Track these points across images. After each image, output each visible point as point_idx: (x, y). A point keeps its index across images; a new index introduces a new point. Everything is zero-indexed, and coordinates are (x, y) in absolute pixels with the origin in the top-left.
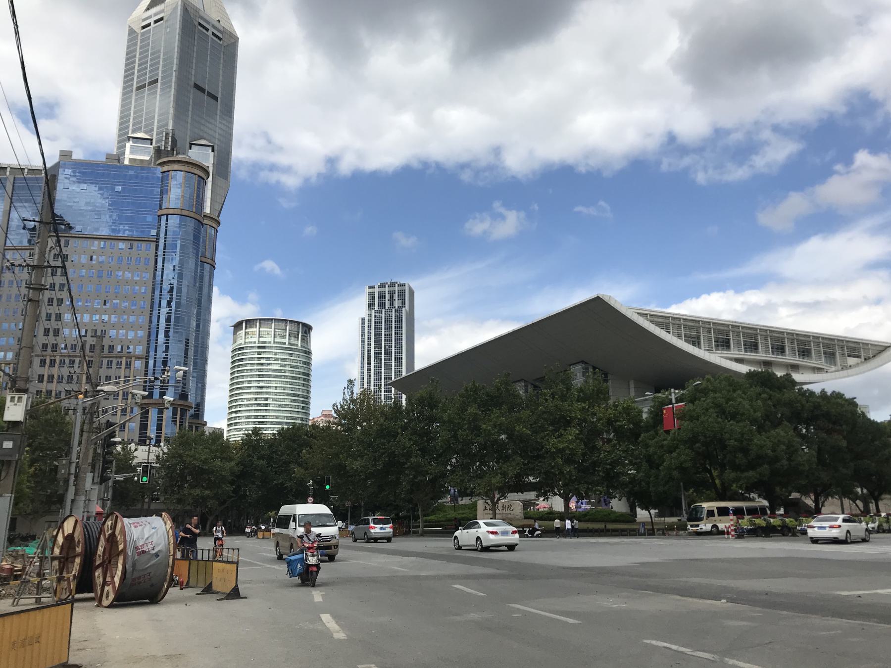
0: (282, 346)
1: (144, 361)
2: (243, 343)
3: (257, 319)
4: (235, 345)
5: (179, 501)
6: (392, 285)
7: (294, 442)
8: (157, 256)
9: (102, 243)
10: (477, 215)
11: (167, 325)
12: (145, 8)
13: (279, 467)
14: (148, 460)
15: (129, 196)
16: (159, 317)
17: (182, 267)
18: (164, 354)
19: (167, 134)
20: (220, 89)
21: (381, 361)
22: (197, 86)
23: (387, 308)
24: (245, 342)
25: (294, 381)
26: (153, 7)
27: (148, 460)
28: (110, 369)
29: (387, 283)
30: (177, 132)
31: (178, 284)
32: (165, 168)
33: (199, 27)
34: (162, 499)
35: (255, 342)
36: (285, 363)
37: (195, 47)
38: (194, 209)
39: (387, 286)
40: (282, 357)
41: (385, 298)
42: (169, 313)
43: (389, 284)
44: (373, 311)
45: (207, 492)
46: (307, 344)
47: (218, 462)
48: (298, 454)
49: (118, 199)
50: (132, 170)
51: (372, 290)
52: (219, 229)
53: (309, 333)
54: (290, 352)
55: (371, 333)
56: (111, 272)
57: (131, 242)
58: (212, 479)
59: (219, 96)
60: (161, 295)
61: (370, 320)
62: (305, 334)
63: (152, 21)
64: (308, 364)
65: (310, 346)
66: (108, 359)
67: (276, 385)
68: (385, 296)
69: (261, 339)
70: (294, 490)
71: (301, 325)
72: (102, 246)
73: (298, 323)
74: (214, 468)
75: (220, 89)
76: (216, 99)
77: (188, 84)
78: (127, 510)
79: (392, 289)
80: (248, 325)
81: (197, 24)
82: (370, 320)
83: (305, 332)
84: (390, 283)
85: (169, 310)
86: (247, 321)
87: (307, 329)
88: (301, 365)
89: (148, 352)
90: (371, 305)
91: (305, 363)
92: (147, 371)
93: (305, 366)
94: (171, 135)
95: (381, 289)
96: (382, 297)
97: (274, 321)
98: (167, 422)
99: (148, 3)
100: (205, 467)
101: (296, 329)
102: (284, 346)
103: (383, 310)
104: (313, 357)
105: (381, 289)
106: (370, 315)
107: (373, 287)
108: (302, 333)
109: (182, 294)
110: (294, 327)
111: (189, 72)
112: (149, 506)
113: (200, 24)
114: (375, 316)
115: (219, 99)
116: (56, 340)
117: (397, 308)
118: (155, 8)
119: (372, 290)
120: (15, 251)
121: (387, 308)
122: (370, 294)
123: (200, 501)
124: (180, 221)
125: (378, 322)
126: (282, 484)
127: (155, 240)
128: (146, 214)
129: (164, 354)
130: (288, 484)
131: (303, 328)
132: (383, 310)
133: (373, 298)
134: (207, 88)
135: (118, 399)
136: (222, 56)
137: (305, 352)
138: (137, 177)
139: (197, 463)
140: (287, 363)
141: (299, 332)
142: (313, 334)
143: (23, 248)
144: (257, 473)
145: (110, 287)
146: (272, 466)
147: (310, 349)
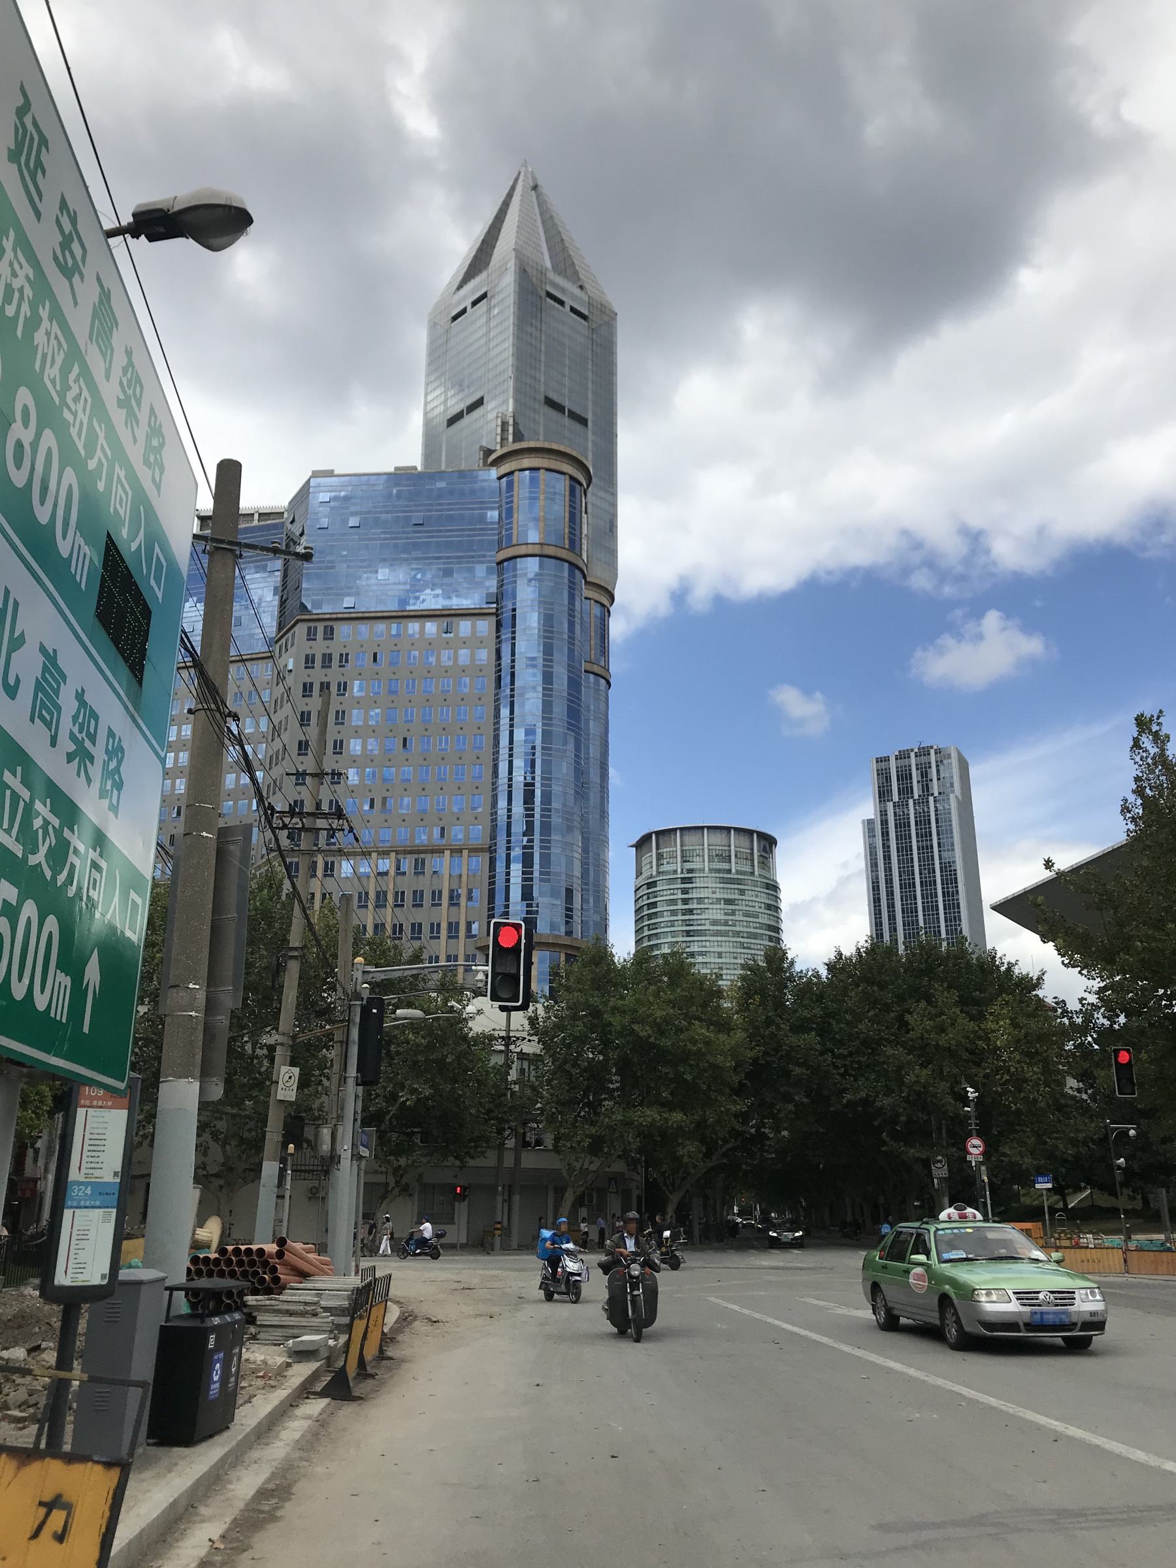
0: (725, 876)
1: (487, 855)
2: (654, 873)
3: (675, 830)
4: (640, 878)
5: (596, 1147)
6: (924, 752)
7: (882, 986)
8: (500, 670)
9: (394, 626)
10: (280, 1428)
11: (526, 809)
12: (456, 286)
13: (851, 1054)
14: (508, 1030)
15: (440, 531)
16: (507, 888)
17: (552, 632)
18: (525, 839)
19: (504, 425)
20: (590, 406)
21: (915, 899)
22: (550, 403)
23: (916, 797)
24: (659, 873)
25: (753, 941)
26: (469, 280)
27: (508, 1030)
28: (421, 877)
29: (912, 750)
30: (521, 421)
31: (543, 725)
32: (505, 468)
33: (548, 300)
34: (549, 1140)
35: (675, 872)
36: (733, 907)
37: (543, 345)
38: (567, 542)
39: (912, 755)
40: (726, 896)
41: (911, 779)
42: (528, 847)
43: (916, 750)
44: (890, 805)
45: (677, 1117)
46: (769, 872)
47: (701, 1031)
48: (900, 1019)
49: (419, 538)
50: (441, 479)
51: (883, 765)
52: (611, 609)
53: (771, 852)
54: (740, 887)
55: (889, 847)
56: (414, 681)
57: (449, 619)
58: (688, 1077)
59: (590, 417)
60: (509, 842)
61: (884, 823)
62: (763, 854)
63: (468, 303)
64: (774, 908)
65: (774, 874)
66: (416, 856)
67: (720, 950)
68: (911, 774)
69: (688, 866)
70: (903, 1119)
71: (755, 836)
72: (394, 632)
73: (750, 833)
74: (690, 1046)
75: (590, 406)
76: (583, 421)
77: (535, 399)
78: (461, 1168)
79: (923, 759)
80: (661, 841)
81: (543, 294)
82: (884, 823)
83: (765, 850)
84: (919, 749)
85: (529, 841)
86: (658, 833)
87: (768, 842)
88: (762, 910)
89: (493, 837)
90: (883, 794)
91: (769, 907)
92: (494, 876)
93: (769, 912)
94: (511, 422)
95: (901, 762)
96: (904, 776)
97: (706, 830)
98: (540, 973)
99: (461, 278)
100: (666, 1043)
101: (747, 844)
102: (728, 876)
103: (911, 802)
104: (782, 896)
105: (901, 762)
106: (883, 813)
107: (887, 759)
108: (758, 851)
109: (555, 686)
110: (744, 841)
111: (535, 378)
112: (518, 1160)
113: (549, 295)
114: (895, 813)
115: (590, 424)
116: (300, 793)
117: (936, 794)
118: (472, 281)
119: (883, 765)
120: (240, 664)
121: (916, 797)
122: (880, 773)
123: (997, 1060)
124: (541, 566)
125: (902, 825)
126: (865, 1102)
127: (494, 611)
128: (473, 562)
129: (525, 839)
130: (885, 1101)
131: (759, 841)
132: (911, 802)
133: (888, 779)
134: (567, 404)
135: (439, 938)
136: (590, 366)
137: (768, 886)
138: (451, 492)
139: (643, 1031)
140: (737, 907)
141: (752, 849)
142: (778, 851)
143: (254, 656)
144: (798, 1070)
145: (412, 712)
146: (832, 1051)
147: (776, 882)
